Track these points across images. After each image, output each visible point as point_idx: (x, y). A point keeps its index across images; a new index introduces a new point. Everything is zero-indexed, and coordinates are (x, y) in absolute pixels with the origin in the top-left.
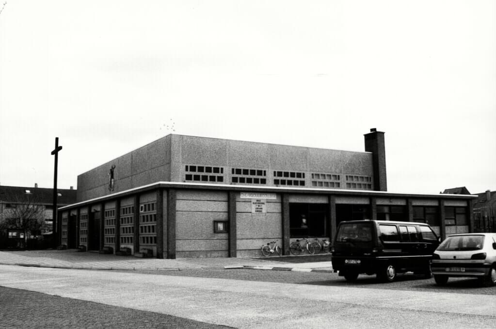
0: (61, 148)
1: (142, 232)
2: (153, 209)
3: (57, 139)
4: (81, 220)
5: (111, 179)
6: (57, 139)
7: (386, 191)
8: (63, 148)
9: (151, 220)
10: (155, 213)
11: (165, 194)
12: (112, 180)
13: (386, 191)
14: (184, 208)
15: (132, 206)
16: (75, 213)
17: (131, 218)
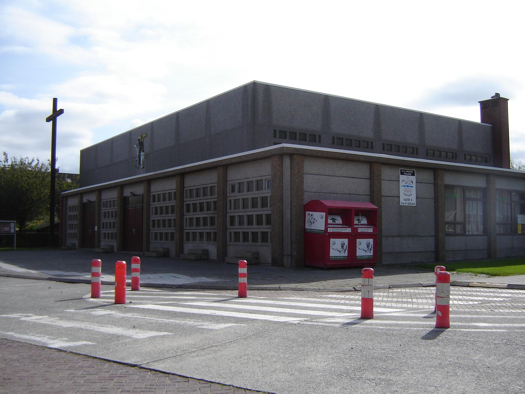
0: (61, 111)
1: (103, 228)
2: (114, 206)
3: (55, 101)
4: (102, 208)
5: (140, 153)
6: (55, 101)
7: (401, 174)
8: (45, 120)
9: (112, 217)
10: (116, 210)
11: (287, 162)
12: (142, 153)
13: (401, 174)
14: (349, 179)
15: (173, 191)
16: (93, 198)
17: (77, 215)
